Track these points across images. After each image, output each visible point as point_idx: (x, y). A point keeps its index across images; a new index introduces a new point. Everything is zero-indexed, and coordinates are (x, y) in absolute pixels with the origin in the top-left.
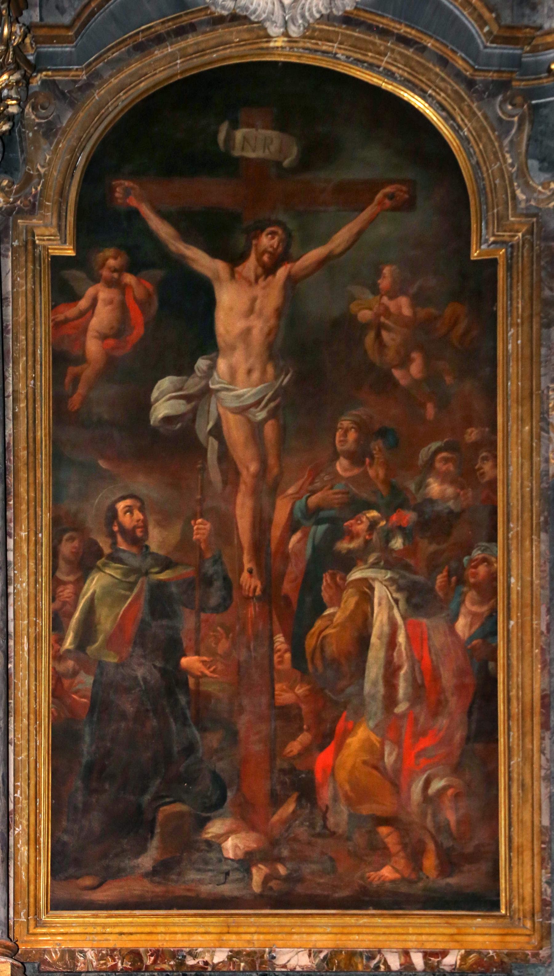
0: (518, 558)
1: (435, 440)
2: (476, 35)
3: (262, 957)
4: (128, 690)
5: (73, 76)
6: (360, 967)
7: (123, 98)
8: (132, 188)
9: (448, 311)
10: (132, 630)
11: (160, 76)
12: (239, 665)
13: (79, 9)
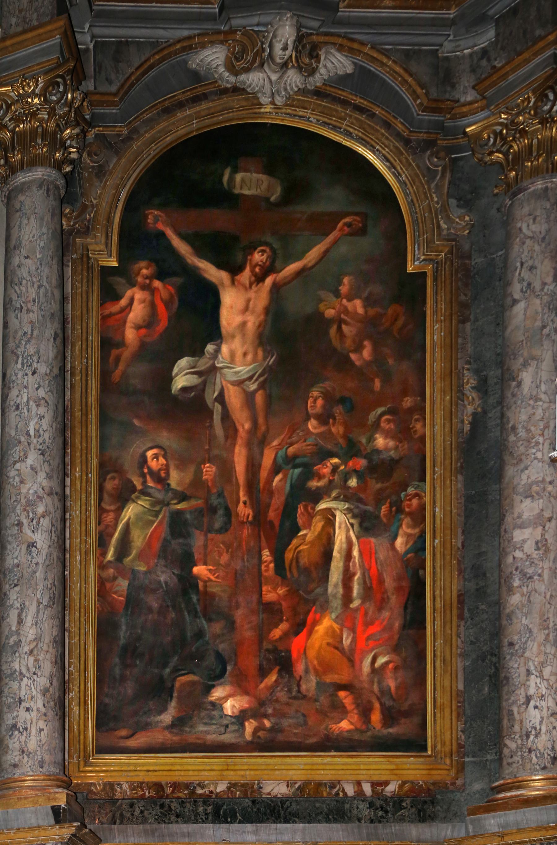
0: (441, 494)
1: (380, 406)
2: (411, 106)
3: (253, 787)
4: (153, 591)
5: (118, 131)
6: (325, 794)
7: (154, 148)
8: (160, 216)
9: (390, 311)
10: (157, 545)
11: (182, 132)
12: (236, 572)
13: (122, 81)
